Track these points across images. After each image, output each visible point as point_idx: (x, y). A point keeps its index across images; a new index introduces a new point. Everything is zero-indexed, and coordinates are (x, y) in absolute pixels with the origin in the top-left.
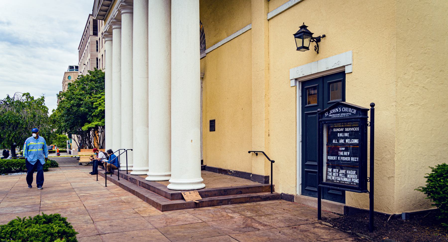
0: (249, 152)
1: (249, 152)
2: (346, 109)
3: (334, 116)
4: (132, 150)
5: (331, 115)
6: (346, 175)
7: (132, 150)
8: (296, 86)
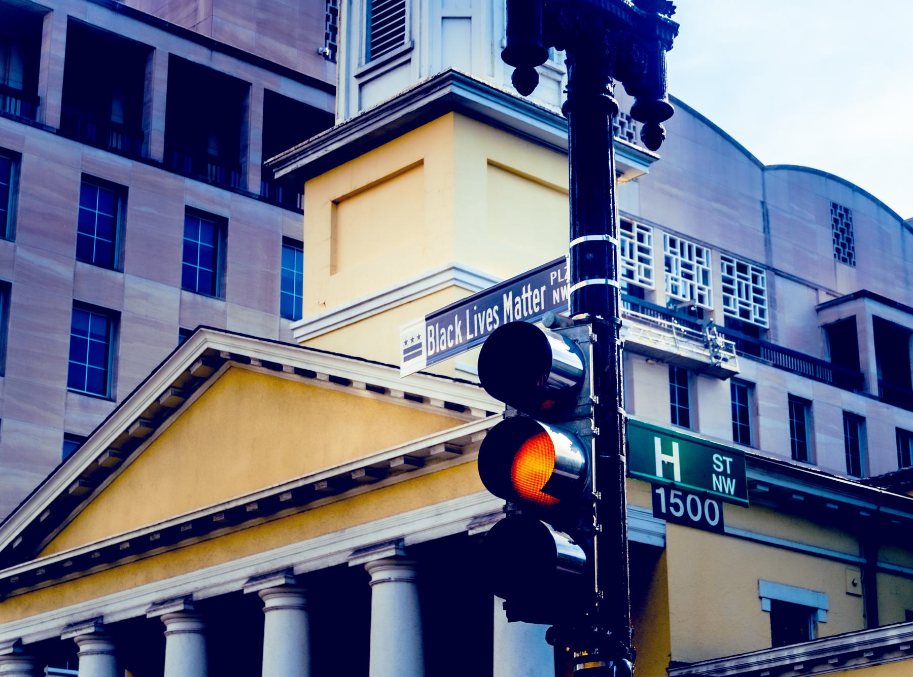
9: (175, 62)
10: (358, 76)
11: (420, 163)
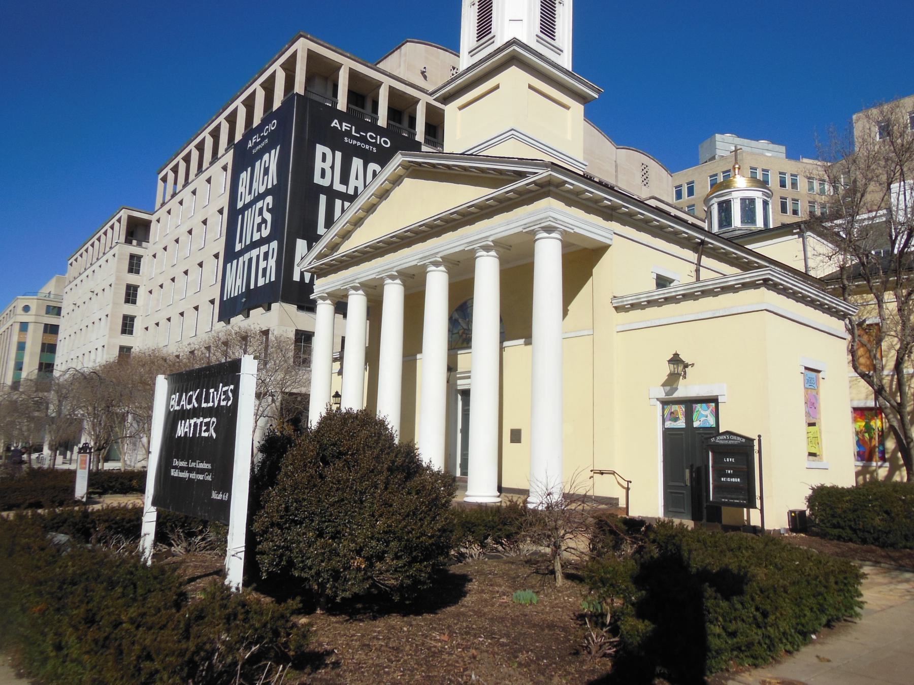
2: (734, 438)
3: (722, 442)
9: (392, 90)
11: (497, 87)
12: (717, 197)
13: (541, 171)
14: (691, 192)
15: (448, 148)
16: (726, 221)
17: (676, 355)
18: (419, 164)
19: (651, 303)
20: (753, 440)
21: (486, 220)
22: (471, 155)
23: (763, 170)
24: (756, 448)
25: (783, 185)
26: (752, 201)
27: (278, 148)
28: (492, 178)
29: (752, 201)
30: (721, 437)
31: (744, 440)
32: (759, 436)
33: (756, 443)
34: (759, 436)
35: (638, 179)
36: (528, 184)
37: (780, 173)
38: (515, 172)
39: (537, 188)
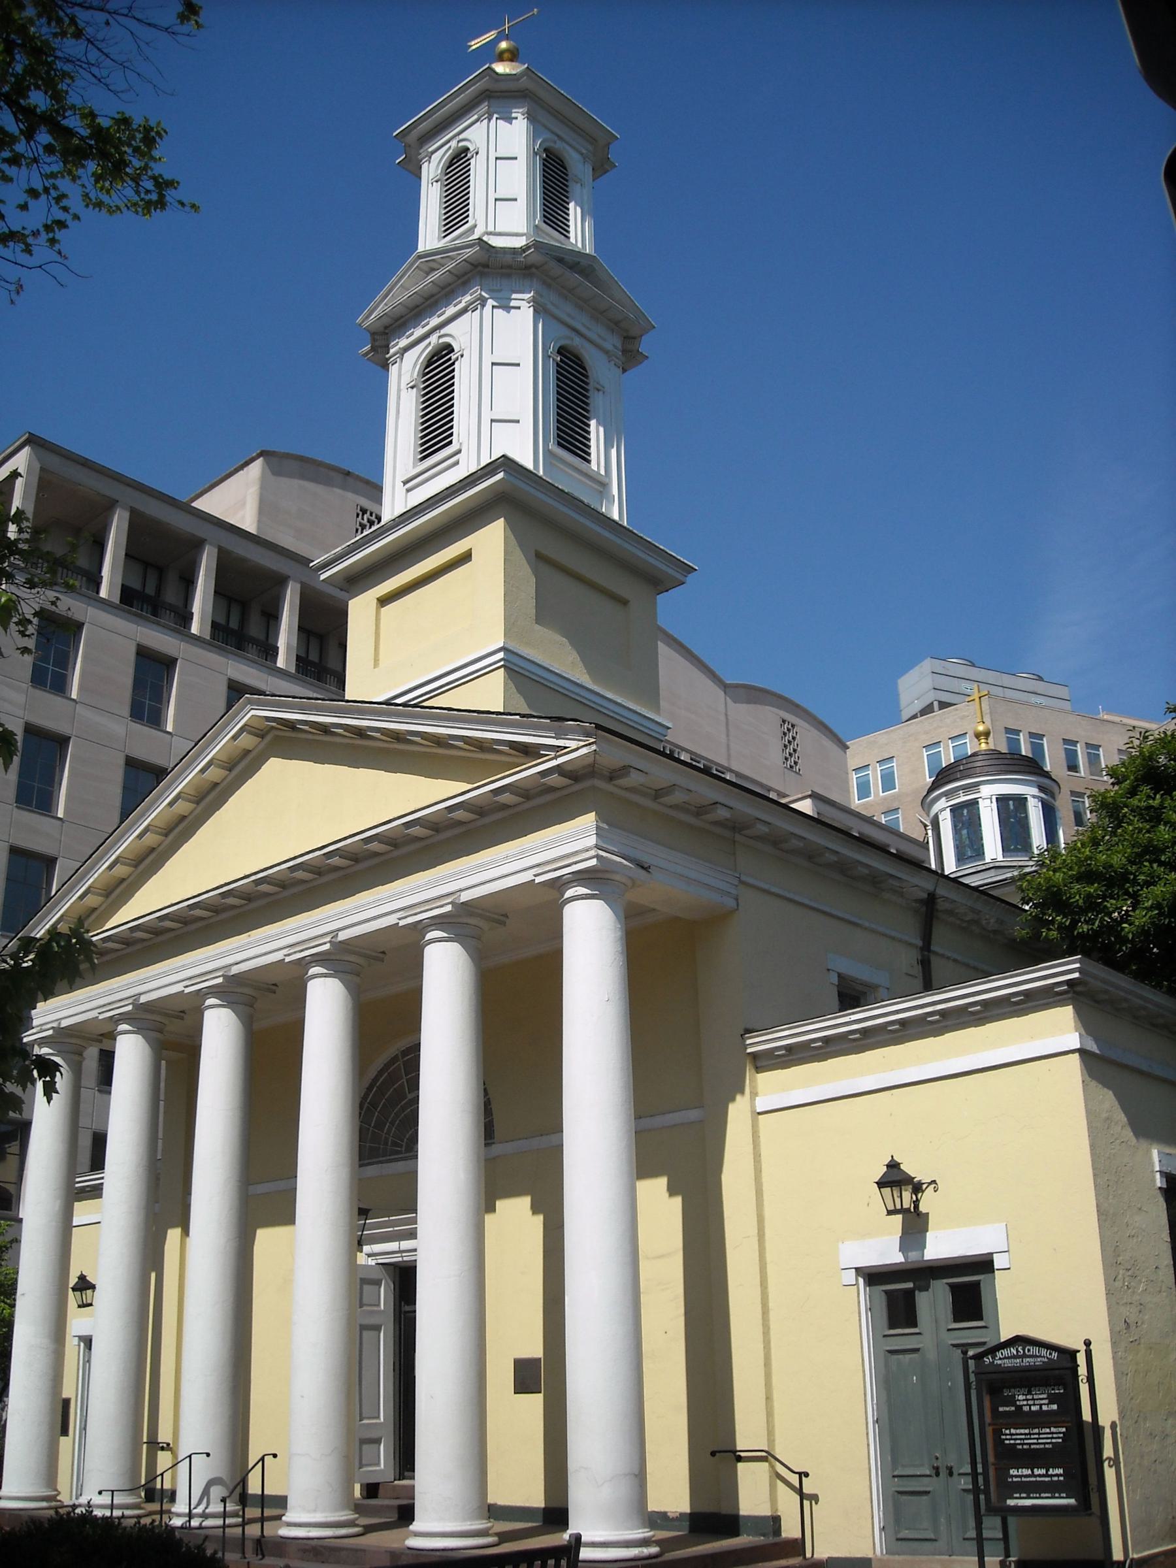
0: (713, 1454)
1: (713, 1454)
2: (1034, 1350)
3: (1008, 1363)
4: (275, 1456)
5: (999, 1362)
6: (1110, 1466)
7: (275, 1456)
8: (857, 1284)
10: (405, 483)
11: (466, 557)
12: (948, 795)
13: (573, 744)
14: (888, 781)
15: (354, 690)
16: (971, 845)
17: (893, 1166)
18: (291, 725)
19: (461, 890)
20: (1073, 1354)
21: (930, 1040)
22: (404, 705)
23: (1032, 735)
24: (1082, 1371)
25: (1073, 767)
26: (1021, 801)
27: (1072, 1501)
28: (381, 749)
29: (1021, 801)
30: (1006, 1352)
31: (1055, 1355)
32: (1088, 1343)
33: (1081, 1359)
34: (1088, 1343)
35: (776, 755)
36: (543, 774)
37: (1066, 741)
38: (513, 745)
39: (566, 781)
